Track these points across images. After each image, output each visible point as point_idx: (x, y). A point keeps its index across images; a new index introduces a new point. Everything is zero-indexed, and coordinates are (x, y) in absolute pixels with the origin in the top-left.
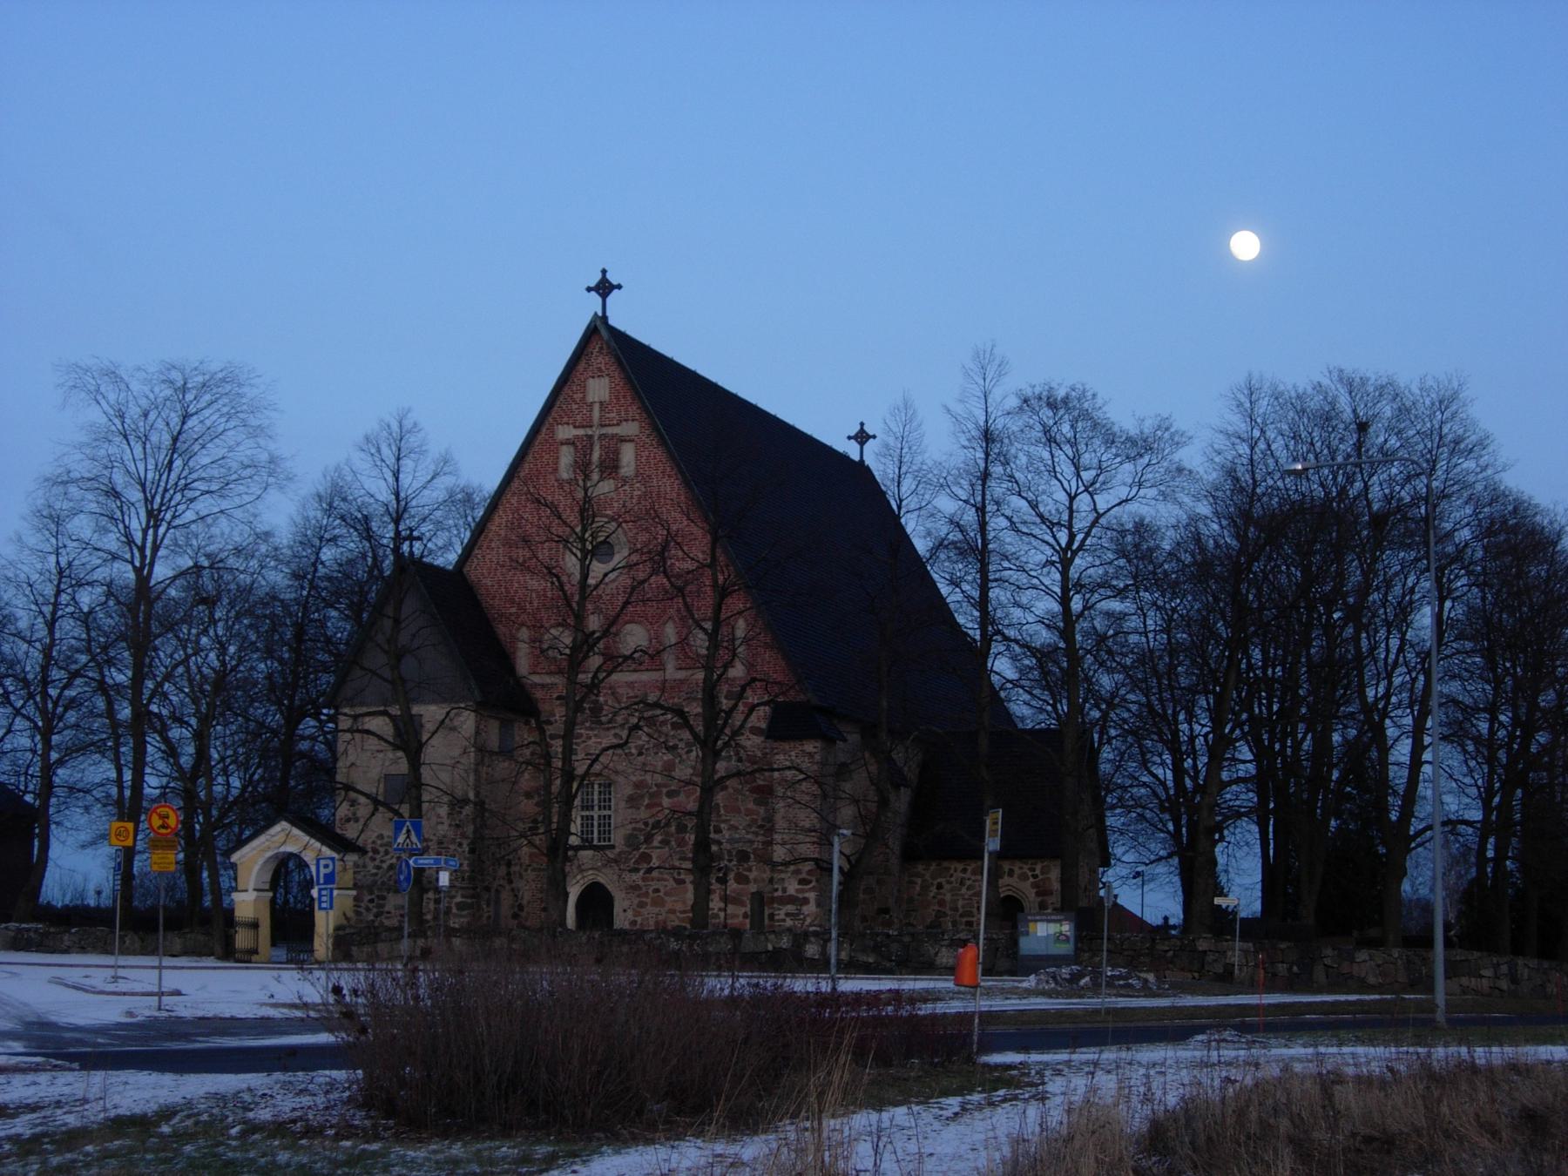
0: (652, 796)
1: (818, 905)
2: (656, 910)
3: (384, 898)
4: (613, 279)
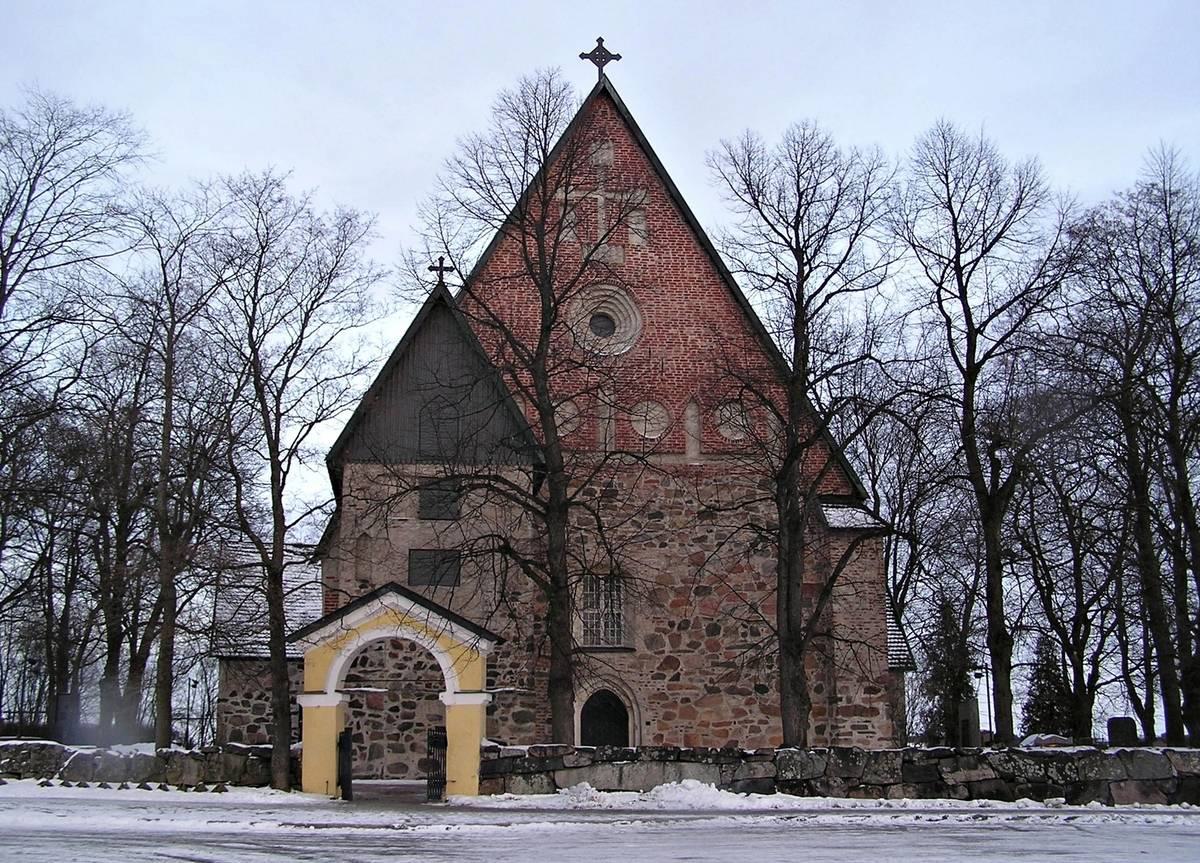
0: (678, 592)
1: (891, 716)
2: (686, 723)
3: (412, 706)
4: (590, 46)
